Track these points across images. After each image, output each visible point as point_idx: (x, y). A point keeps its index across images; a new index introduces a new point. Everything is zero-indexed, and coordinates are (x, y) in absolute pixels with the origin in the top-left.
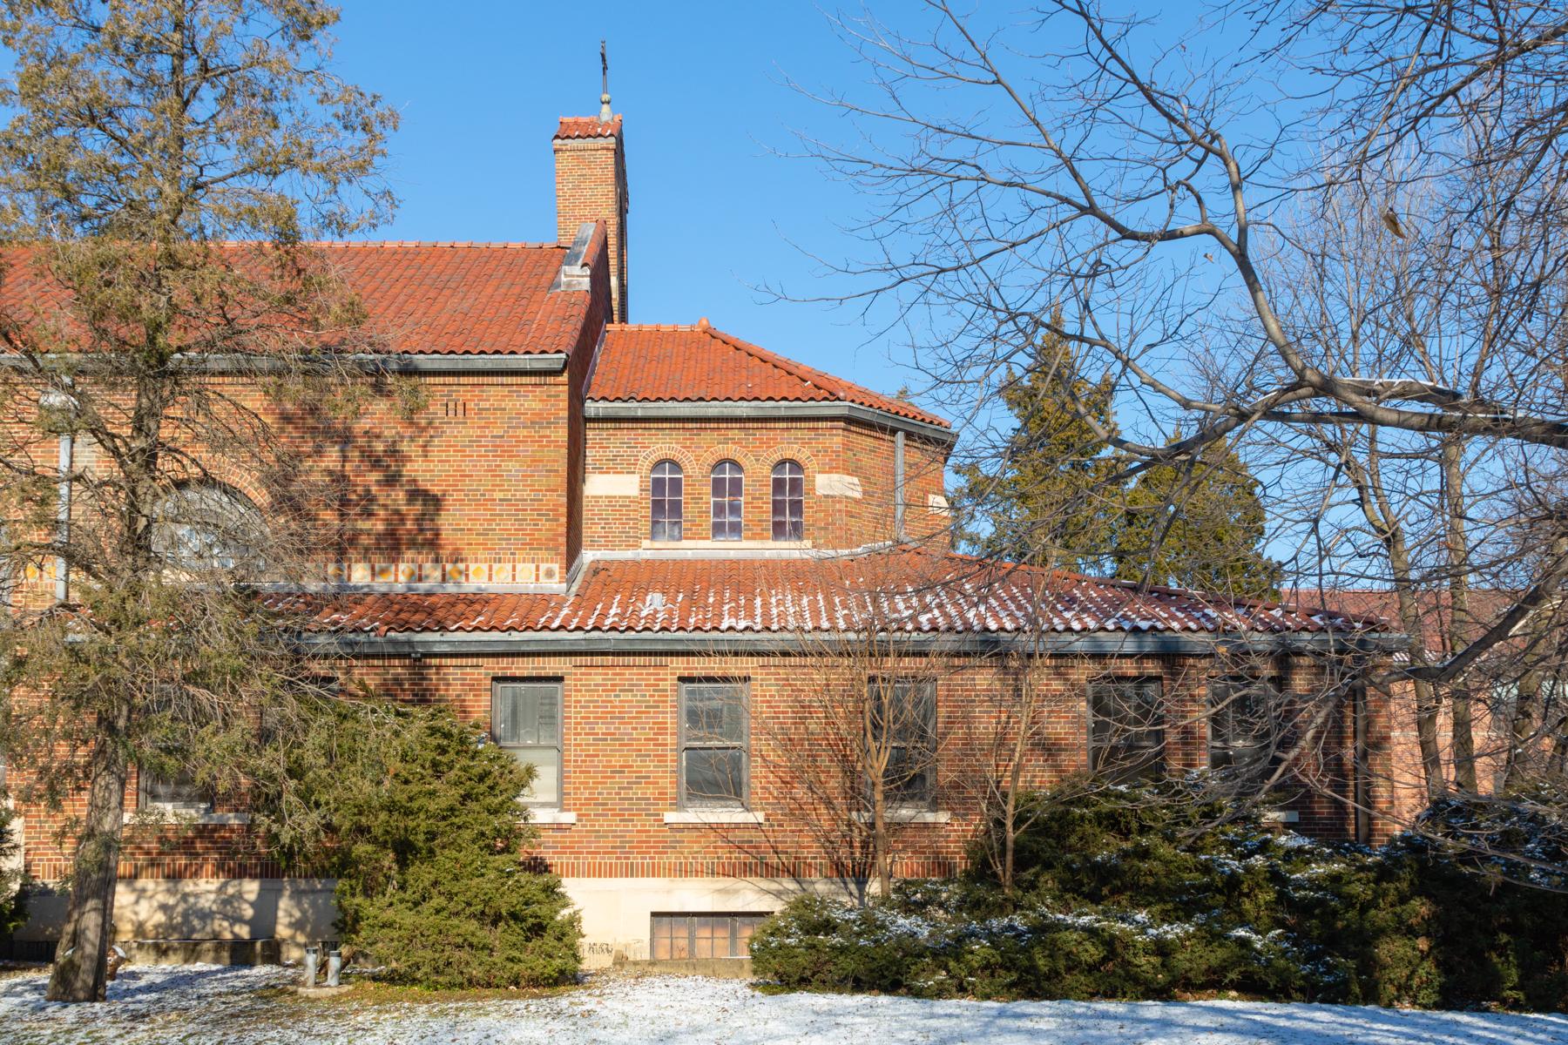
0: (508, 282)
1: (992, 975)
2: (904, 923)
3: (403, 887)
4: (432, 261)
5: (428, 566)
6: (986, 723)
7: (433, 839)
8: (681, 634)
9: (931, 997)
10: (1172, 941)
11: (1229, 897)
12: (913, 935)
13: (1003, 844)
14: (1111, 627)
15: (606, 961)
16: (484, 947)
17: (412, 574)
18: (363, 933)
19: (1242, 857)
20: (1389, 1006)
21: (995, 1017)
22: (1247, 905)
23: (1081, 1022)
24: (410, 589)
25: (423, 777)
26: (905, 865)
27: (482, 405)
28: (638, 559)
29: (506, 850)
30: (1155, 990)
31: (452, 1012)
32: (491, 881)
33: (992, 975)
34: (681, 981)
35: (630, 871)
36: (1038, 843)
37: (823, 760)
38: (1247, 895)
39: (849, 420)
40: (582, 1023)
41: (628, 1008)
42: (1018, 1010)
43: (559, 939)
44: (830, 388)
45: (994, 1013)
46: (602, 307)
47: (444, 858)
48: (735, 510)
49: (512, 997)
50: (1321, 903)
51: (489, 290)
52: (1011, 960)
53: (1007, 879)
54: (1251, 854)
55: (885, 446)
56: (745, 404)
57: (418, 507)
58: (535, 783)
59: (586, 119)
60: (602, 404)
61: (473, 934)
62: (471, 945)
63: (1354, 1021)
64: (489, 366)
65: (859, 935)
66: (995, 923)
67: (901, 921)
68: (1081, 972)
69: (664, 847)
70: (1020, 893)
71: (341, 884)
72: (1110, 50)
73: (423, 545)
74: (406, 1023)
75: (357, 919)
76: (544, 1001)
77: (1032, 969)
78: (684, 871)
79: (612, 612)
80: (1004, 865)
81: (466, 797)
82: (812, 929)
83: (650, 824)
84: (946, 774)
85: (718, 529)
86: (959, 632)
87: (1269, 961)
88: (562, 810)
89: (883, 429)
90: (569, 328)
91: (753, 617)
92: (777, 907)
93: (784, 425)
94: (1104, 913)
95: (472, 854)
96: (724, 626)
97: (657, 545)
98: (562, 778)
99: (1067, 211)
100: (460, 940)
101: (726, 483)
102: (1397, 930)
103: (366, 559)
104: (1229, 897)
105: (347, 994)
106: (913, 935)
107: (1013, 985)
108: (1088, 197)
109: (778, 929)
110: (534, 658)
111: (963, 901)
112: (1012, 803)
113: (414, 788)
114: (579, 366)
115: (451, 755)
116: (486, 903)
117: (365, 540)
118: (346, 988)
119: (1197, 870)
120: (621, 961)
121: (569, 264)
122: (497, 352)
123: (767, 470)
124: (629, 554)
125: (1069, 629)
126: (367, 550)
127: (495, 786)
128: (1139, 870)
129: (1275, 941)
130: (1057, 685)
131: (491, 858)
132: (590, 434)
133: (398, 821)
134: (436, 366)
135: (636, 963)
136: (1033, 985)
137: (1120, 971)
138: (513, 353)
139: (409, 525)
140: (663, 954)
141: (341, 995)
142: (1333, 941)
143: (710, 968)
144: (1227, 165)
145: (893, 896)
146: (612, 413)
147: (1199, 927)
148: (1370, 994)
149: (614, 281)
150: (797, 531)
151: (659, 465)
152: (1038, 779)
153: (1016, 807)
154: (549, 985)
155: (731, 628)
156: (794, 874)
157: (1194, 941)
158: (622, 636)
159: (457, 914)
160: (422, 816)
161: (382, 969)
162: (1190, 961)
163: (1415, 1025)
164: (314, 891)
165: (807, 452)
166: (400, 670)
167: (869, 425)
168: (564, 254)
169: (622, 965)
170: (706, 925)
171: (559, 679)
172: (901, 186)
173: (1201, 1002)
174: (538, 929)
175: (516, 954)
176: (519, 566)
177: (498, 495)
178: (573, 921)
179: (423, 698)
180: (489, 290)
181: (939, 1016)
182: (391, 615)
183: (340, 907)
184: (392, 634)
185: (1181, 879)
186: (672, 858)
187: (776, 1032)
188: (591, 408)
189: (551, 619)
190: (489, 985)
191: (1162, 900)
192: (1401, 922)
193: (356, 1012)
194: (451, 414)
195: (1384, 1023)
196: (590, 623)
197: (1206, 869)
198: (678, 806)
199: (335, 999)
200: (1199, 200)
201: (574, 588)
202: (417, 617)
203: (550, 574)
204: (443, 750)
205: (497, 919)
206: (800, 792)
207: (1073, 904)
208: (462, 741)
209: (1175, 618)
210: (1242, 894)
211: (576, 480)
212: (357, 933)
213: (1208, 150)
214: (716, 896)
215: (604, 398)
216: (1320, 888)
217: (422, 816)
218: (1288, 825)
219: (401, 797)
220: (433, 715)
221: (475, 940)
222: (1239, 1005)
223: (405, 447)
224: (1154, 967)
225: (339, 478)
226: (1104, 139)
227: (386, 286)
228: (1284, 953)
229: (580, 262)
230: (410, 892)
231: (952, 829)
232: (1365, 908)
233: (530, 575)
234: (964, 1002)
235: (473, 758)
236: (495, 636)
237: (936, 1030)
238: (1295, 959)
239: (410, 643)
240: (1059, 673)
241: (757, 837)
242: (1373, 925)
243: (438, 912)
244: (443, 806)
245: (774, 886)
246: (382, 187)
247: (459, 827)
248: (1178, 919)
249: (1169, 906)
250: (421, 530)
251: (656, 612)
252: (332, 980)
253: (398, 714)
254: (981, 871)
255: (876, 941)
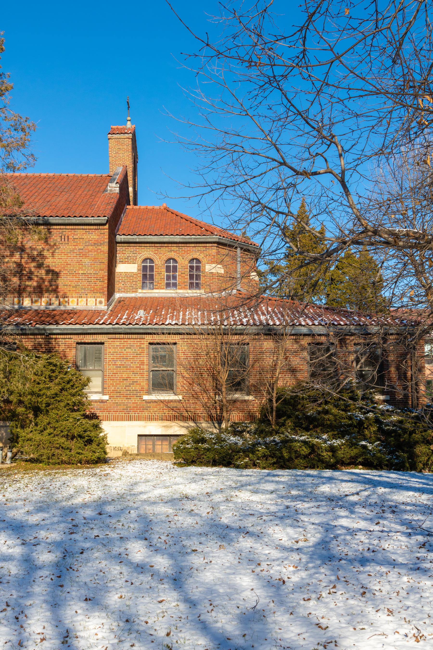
0: (87, 190)
1: (266, 460)
2: (233, 439)
3: (36, 425)
4: (59, 181)
5: (53, 299)
6: (268, 361)
7: (49, 406)
8: (150, 326)
9: (243, 468)
10: (336, 446)
11: (360, 429)
12: (236, 444)
13: (272, 408)
14: (317, 324)
15: (120, 454)
16: (68, 448)
17: (48, 302)
18: (20, 443)
19: (365, 413)
20: (420, 471)
21: (265, 476)
22: (366, 432)
23: (298, 478)
24: (46, 308)
25: (45, 382)
26: (236, 416)
27: (75, 237)
28: (137, 297)
29: (78, 410)
30: (330, 465)
31: (53, 474)
32: (72, 422)
33: (266, 460)
34: (147, 462)
35: (130, 419)
36: (285, 408)
37: (205, 375)
38: (366, 428)
39: (219, 243)
40: (104, 478)
41: (123, 473)
42: (275, 473)
43: (98, 445)
44: (212, 231)
45: (266, 474)
46: (124, 199)
47: (53, 414)
48: (174, 278)
49: (78, 468)
50: (394, 431)
51: (80, 192)
52: (273, 454)
53: (273, 422)
54: (368, 412)
55: (232, 253)
56: (178, 237)
57: (50, 276)
58: (90, 384)
59: (121, 127)
60: (123, 237)
61: (63, 443)
62: (62, 448)
63: (404, 478)
64: (78, 222)
65: (215, 444)
66: (268, 439)
67: (232, 438)
68: (301, 458)
69: (143, 409)
70: (278, 427)
71: (12, 424)
72: (290, 102)
73: (51, 291)
74: (33, 479)
75: (18, 437)
76: (90, 470)
77: (282, 457)
78: (151, 419)
79: (124, 317)
80: (272, 417)
81: (62, 390)
82: (197, 441)
83: (138, 400)
84: (252, 381)
85: (168, 285)
86: (258, 326)
87: (374, 454)
88: (103, 395)
89: (230, 246)
90: (109, 207)
91: (178, 319)
92: (183, 431)
93: (194, 245)
94: (310, 435)
95: (64, 412)
96: (167, 323)
97: (144, 291)
98: (103, 382)
99: (276, 164)
100: (58, 446)
101: (171, 268)
102: (423, 442)
103: (29, 296)
104: (360, 429)
105: (14, 467)
106: (236, 444)
107: (274, 463)
108: (283, 158)
109: (184, 441)
110: (93, 335)
111: (256, 430)
112: (275, 392)
113: (41, 386)
114: (114, 222)
115: (57, 373)
116: (69, 431)
117: (29, 289)
118: (14, 464)
119: (347, 418)
120: (125, 454)
121: (111, 183)
122: (81, 216)
123: (187, 262)
124: (133, 295)
125: (300, 325)
126: (30, 293)
127: (75, 385)
128: (324, 418)
129: (377, 446)
130: (296, 346)
131: (71, 414)
132: (118, 248)
133: (34, 399)
134: (57, 222)
135: (131, 455)
136: (282, 463)
137: (316, 458)
138: (87, 217)
139: (46, 283)
140: (143, 451)
141: (11, 467)
142: (400, 446)
143: (160, 457)
144: (337, 147)
145: (229, 429)
146: (127, 240)
147: (347, 441)
148: (413, 467)
149: (131, 189)
150: (198, 286)
151: (145, 260)
152: (285, 382)
153: (277, 394)
154: (94, 463)
155: (176, 324)
156: (194, 420)
157: (345, 446)
158: (127, 327)
159: (57, 435)
160: (44, 397)
161: (28, 457)
162: (343, 454)
163: (427, 479)
164: (6, 426)
165: (202, 255)
166: (40, 340)
167: (224, 245)
168: (111, 179)
169: (125, 455)
170: (159, 440)
171: (102, 343)
172: (213, 154)
173: (347, 470)
174: (90, 441)
175: (81, 451)
176: (89, 299)
177: (81, 272)
178: (104, 438)
179: (49, 351)
180: (80, 192)
181: (244, 476)
182: (38, 318)
183: (11, 432)
184: (38, 326)
185: (341, 422)
186: (146, 414)
187: (178, 482)
188: (119, 238)
189: (100, 320)
190: (69, 463)
191: (333, 430)
192: (424, 439)
193: (15, 474)
194: (63, 240)
195: (416, 478)
196: (115, 321)
197: (350, 418)
198: (148, 393)
199: (9, 469)
200: (326, 160)
201: (110, 308)
202: (48, 319)
203: (101, 302)
204: (53, 371)
205: (73, 437)
206: (197, 388)
207: (299, 431)
208: (61, 368)
209: (342, 320)
210: (364, 428)
211: (112, 266)
212: (18, 443)
213: (331, 142)
214: (163, 428)
215: (124, 235)
216: (394, 425)
217: (44, 397)
218: (384, 401)
219: (36, 390)
220: (50, 357)
221: (64, 446)
222: (362, 471)
223: (45, 253)
224: (329, 456)
225: (19, 265)
226: (287, 136)
227: (40, 191)
228: (380, 451)
229: (115, 182)
230: (39, 427)
231: (254, 402)
232: (411, 433)
233: (94, 303)
234: (255, 470)
235: (65, 374)
236: (78, 326)
237: (241, 481)
238: (384, 454)
239: (44, 329)
240: (296, 341)
241: (179, 405)
242: (414, 440)
243: (49, 434)
244: (52, 393)
245: (186, 425)
246: (29, 153)
247: (59, 401)
248: (339, 438)
249: (336, 433)
250: (51, 285)
251: (141, 317)
252: (8, 461)
253: (36, 357)
254: (264, 420)
255: (221, 446)
